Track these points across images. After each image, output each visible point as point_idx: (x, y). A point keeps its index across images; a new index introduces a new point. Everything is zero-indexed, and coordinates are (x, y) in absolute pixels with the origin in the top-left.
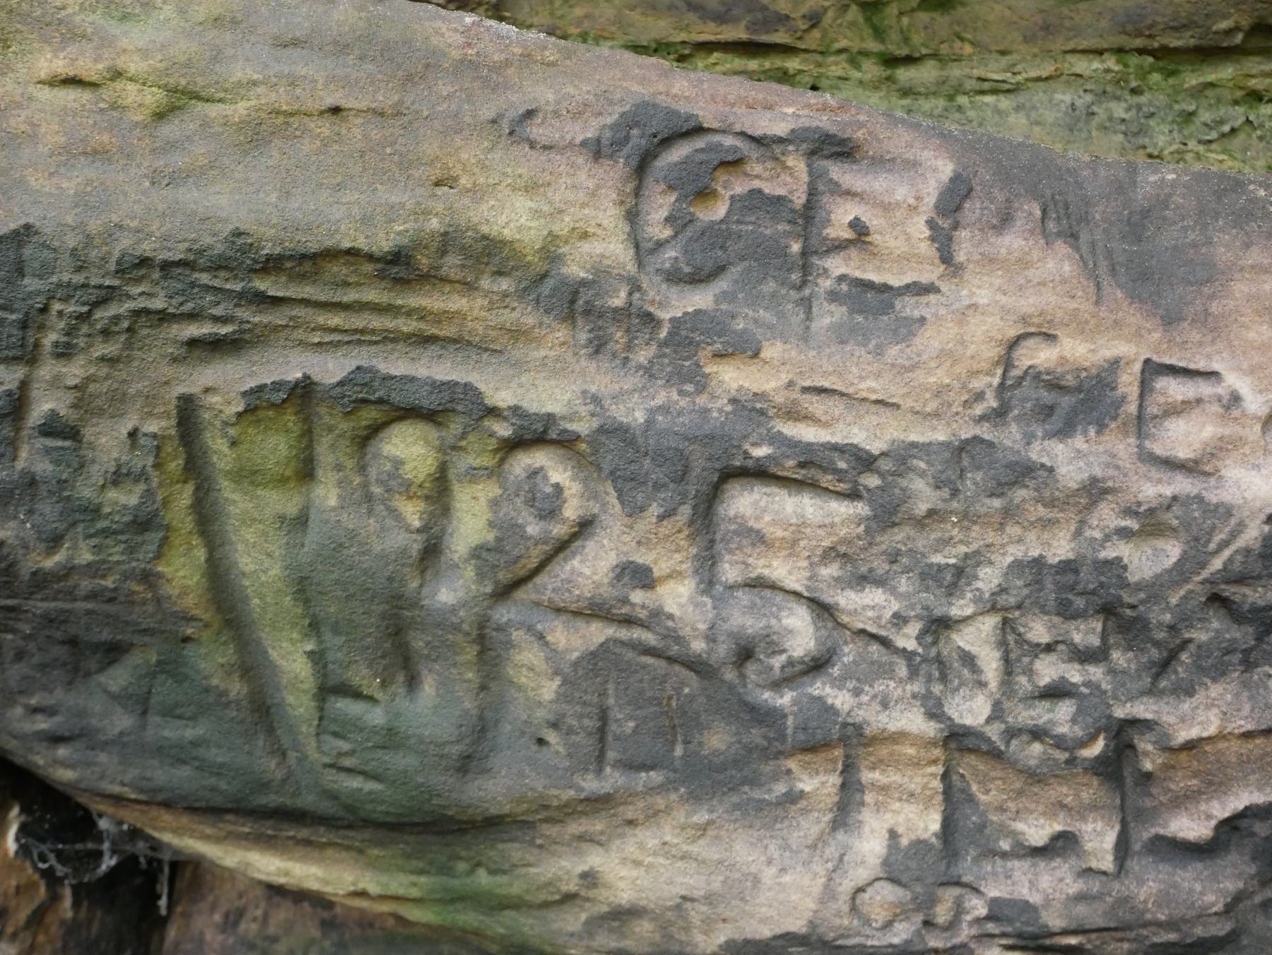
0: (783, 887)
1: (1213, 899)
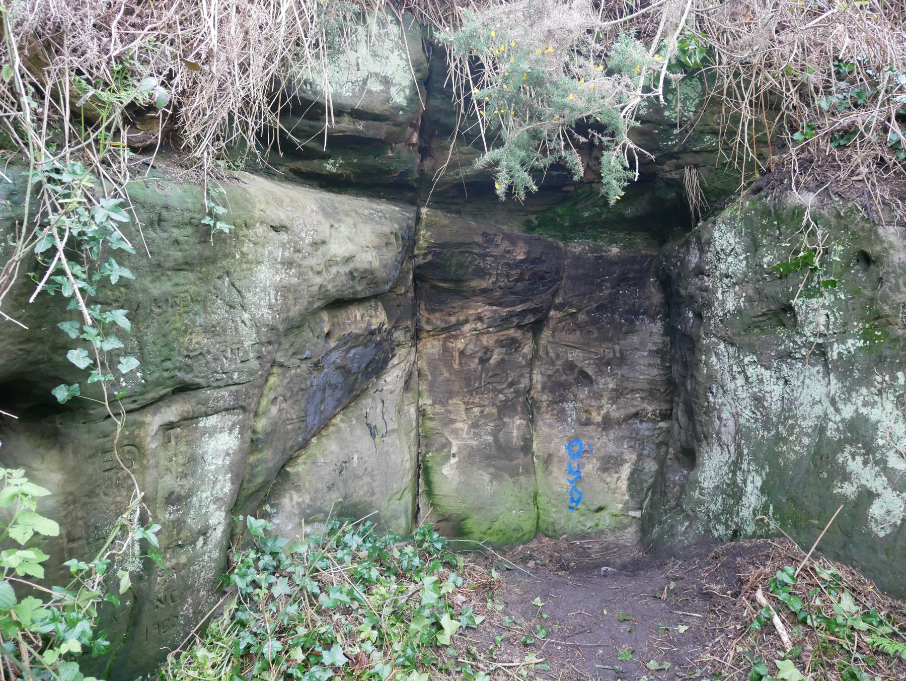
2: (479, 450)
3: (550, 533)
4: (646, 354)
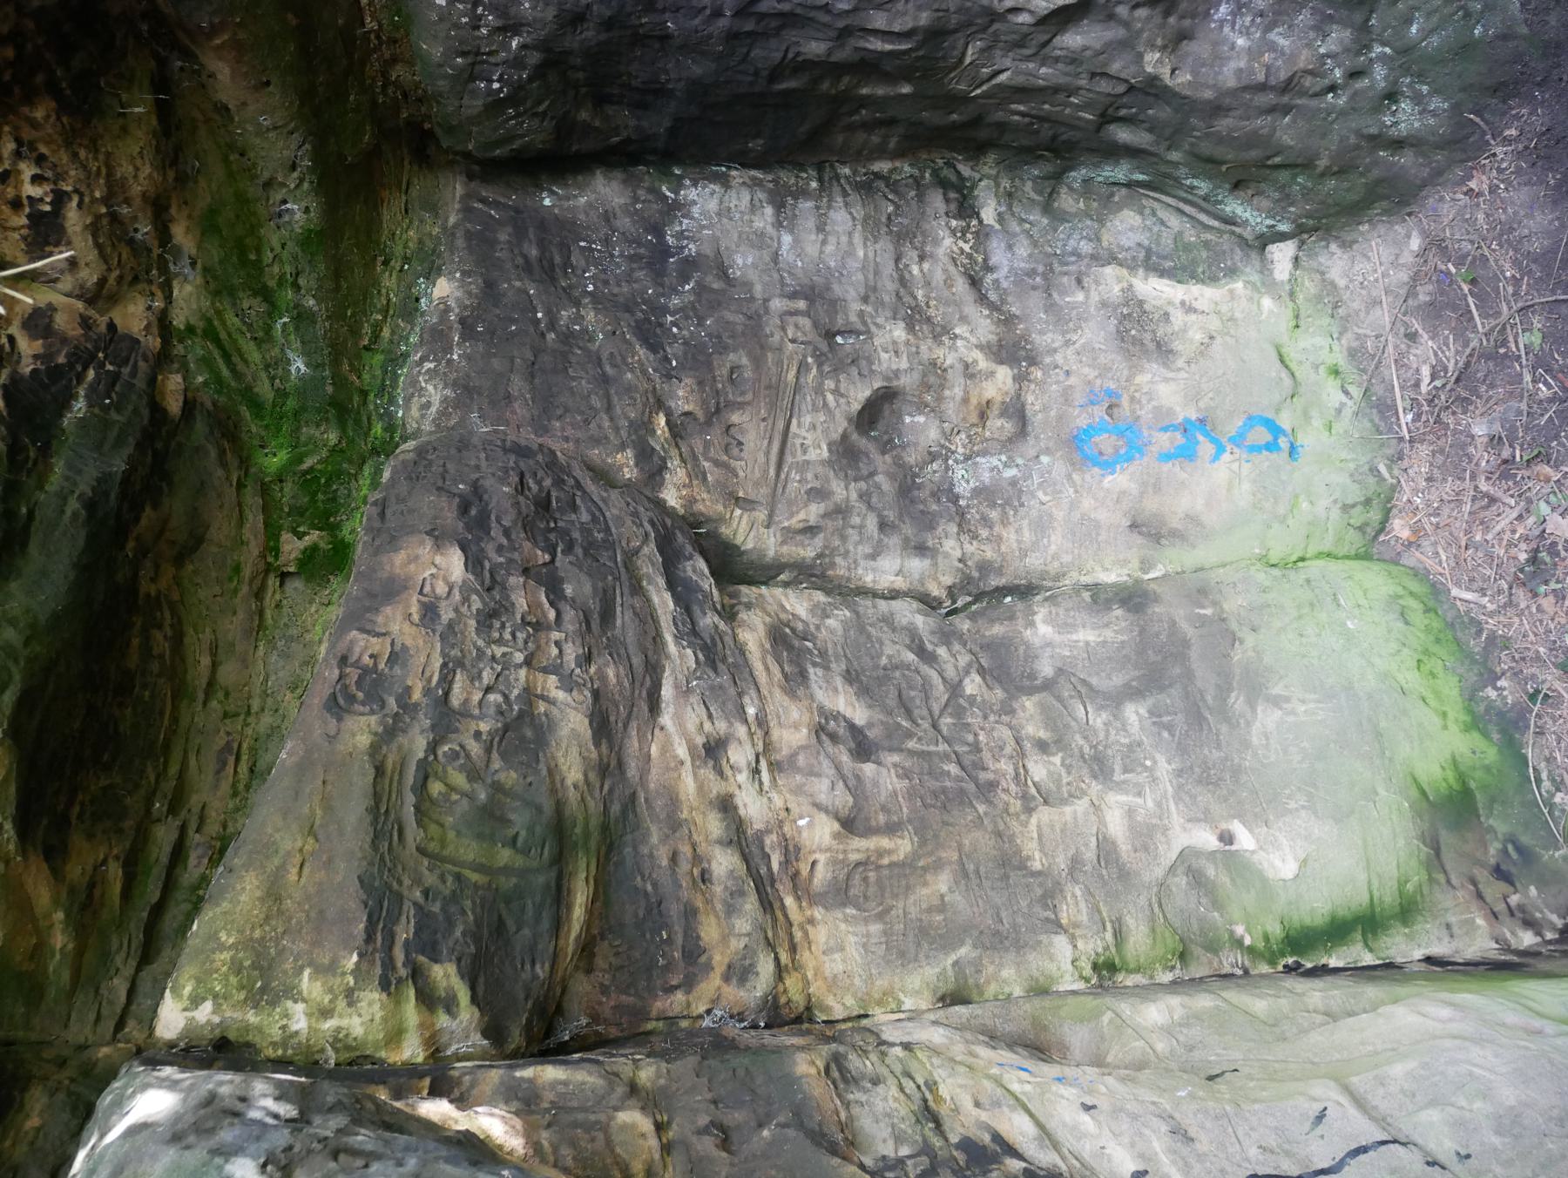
1: (573, 612)
2: (1182, 750)
3: (1375, 516)
4: (787, 239)
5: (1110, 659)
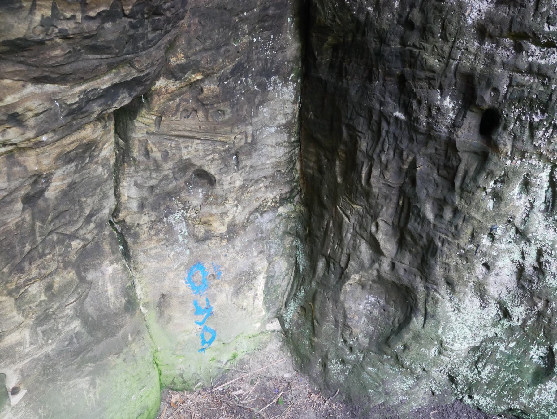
0: (19, 28)
1: (95, 27)
3: (179, 386)
5: (101, 303)
